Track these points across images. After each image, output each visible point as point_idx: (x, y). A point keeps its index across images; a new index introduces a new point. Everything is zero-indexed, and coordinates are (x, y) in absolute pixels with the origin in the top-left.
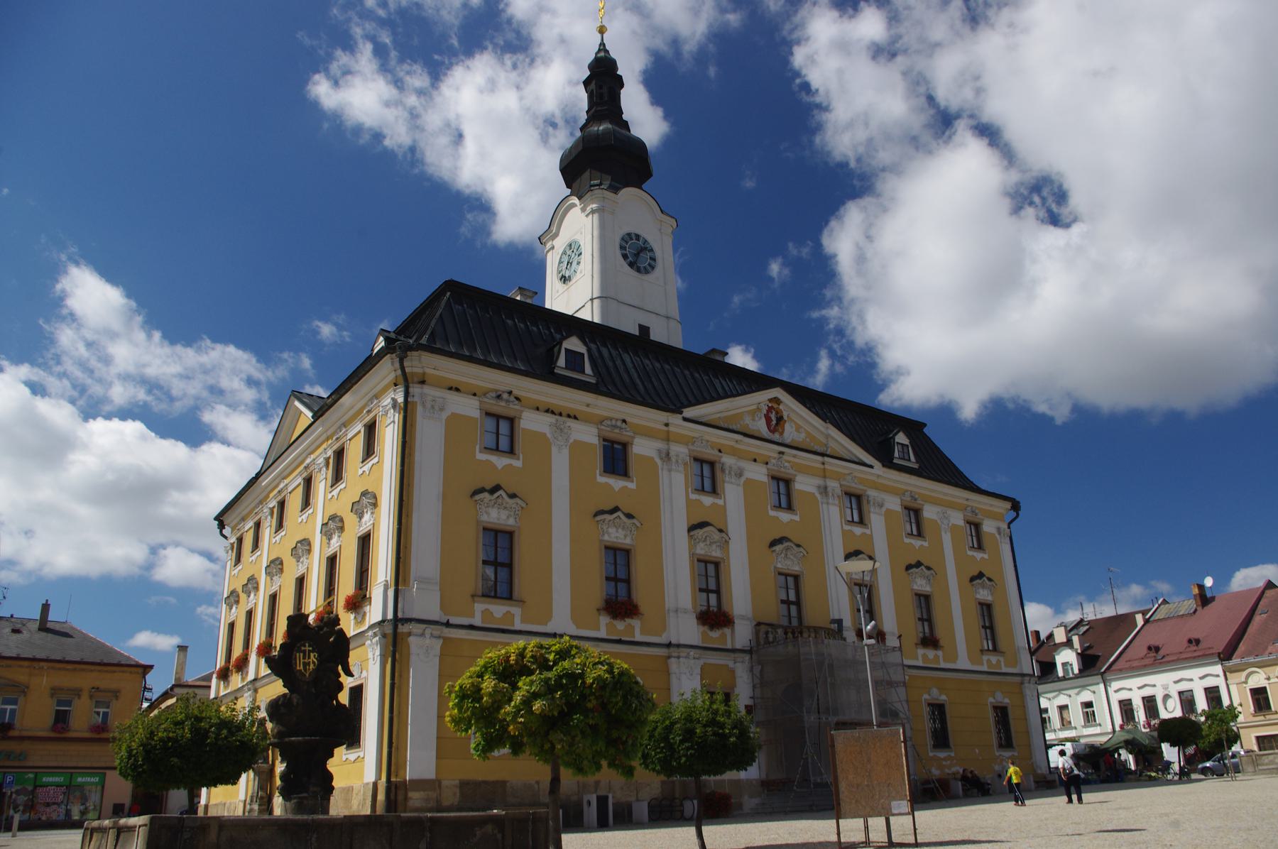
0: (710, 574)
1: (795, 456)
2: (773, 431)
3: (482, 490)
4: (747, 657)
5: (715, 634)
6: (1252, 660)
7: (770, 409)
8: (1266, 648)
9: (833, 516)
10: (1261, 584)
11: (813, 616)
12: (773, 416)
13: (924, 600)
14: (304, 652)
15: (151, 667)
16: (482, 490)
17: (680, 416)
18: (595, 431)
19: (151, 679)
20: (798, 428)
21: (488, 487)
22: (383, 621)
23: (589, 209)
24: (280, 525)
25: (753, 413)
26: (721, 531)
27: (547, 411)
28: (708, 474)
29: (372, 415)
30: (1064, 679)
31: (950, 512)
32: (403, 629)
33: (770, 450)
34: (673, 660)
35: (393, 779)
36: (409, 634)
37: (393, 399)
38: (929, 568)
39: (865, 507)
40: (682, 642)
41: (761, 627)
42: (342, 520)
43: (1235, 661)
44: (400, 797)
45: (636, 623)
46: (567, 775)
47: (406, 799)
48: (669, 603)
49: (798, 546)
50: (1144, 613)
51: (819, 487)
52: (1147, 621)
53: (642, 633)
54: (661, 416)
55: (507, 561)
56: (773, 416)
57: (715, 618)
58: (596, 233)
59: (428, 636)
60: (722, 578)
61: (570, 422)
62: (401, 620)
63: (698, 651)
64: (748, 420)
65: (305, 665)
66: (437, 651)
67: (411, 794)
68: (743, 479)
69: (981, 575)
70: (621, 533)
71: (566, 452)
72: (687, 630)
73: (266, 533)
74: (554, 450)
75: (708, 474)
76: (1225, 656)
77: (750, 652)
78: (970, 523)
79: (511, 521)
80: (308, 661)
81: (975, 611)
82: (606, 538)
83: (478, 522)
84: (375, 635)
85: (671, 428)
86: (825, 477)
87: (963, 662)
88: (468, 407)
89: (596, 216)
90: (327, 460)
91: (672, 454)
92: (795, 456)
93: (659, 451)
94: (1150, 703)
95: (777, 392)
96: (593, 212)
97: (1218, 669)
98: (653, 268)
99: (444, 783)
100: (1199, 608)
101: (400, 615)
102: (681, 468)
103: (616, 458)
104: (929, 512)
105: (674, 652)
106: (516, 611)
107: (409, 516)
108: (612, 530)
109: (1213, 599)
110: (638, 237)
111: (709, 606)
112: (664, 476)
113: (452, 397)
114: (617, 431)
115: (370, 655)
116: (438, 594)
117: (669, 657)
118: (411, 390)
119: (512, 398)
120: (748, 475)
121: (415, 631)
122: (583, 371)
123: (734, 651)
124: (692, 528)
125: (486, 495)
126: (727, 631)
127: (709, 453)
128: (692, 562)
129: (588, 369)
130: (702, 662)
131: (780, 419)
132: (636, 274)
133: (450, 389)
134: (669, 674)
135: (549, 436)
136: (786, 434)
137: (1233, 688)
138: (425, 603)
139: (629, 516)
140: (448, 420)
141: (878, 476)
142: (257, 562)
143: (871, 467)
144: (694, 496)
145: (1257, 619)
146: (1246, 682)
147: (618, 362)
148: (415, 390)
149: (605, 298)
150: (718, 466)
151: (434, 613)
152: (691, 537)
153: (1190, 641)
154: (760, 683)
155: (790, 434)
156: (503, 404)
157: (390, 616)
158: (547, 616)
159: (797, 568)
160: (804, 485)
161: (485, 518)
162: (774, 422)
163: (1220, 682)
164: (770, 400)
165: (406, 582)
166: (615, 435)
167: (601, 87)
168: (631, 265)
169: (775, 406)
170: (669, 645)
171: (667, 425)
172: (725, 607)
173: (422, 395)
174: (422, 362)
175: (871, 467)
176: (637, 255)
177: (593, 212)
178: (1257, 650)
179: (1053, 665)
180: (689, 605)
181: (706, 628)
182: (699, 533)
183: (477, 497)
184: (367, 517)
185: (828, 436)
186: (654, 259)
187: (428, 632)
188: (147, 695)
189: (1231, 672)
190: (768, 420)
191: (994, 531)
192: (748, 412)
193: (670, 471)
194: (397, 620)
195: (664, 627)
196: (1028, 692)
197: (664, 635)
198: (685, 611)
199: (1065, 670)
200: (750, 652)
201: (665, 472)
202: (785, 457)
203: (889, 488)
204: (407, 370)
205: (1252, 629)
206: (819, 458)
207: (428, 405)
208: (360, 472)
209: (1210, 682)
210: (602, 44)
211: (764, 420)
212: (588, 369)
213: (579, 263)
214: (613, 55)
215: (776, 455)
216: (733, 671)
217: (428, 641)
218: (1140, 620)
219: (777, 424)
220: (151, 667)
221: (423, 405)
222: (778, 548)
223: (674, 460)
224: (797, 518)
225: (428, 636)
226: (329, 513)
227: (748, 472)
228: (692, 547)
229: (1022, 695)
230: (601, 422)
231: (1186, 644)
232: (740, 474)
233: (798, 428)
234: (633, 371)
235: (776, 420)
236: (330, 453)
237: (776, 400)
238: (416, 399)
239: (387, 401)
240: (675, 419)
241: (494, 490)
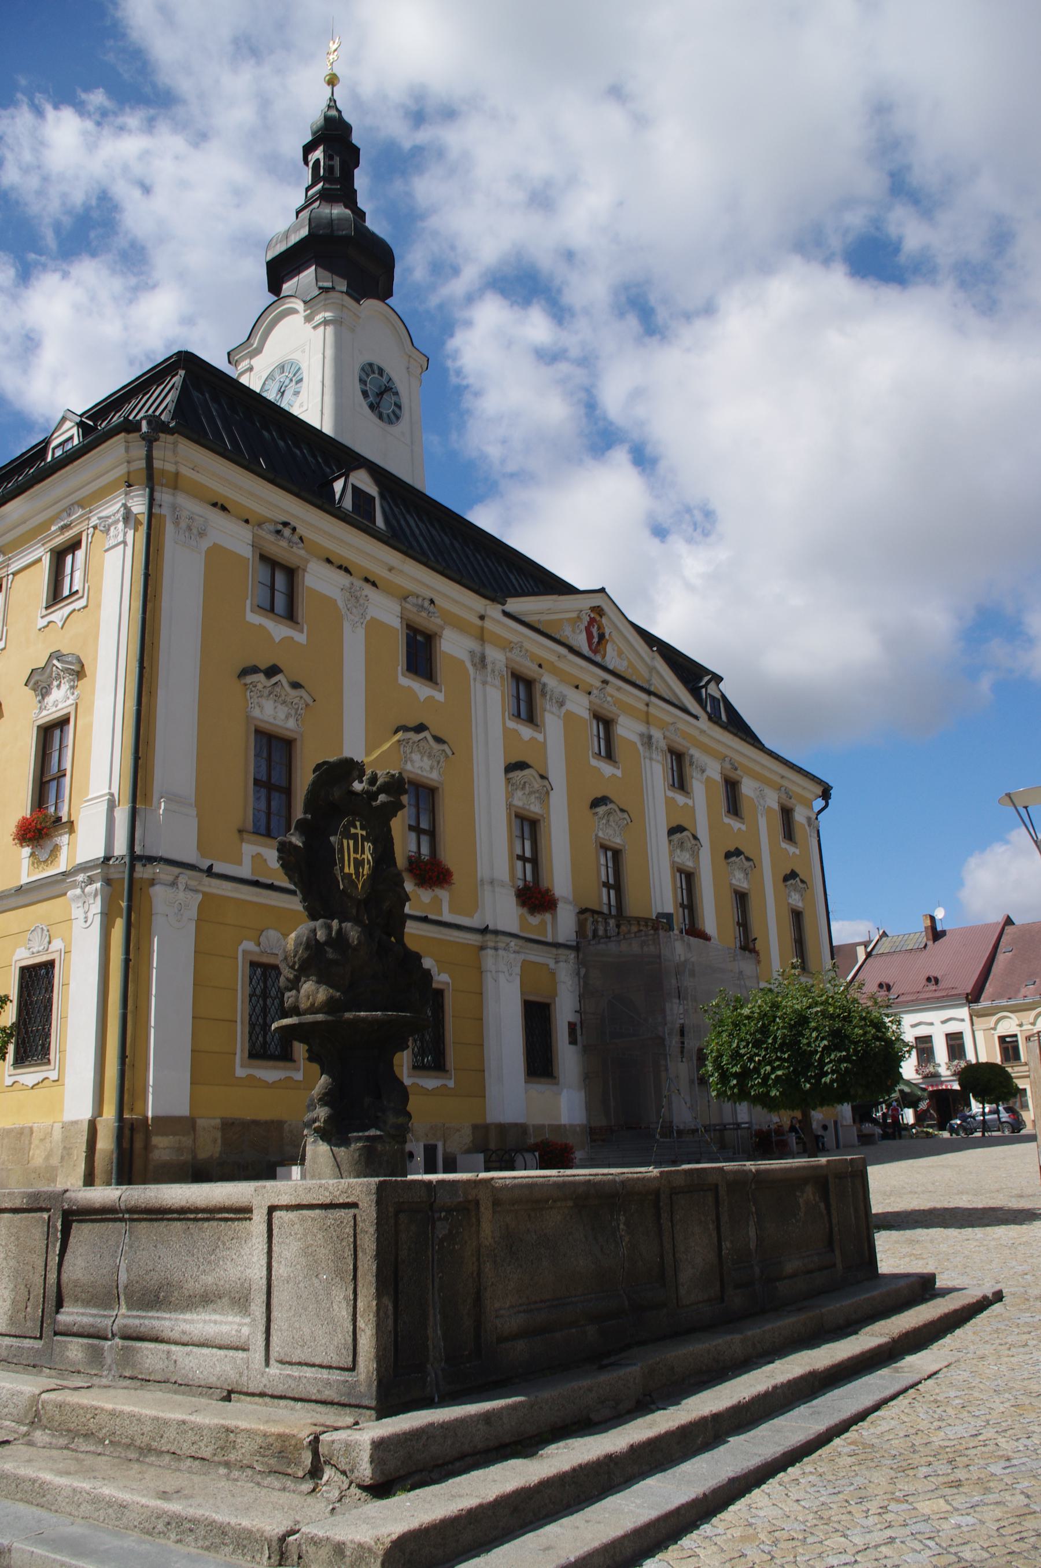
1: (619, 689)
2: (595, 652)
3: (254, 670)
4: (572, 955)
5: (534, 920)
6: (1004, 1002)
7: (592, 621)
8: (1018, 991)
10: (1000, 919)
11: (634, 908)
12: (595, 631)
13: (742, 898)
14: (355, 837)
16: (254, 670)
17: (500, 607)
18: (398, 609)
20: (620, 653)
22: (107, 859)
23: (319, 318)
26: (543, 777)
27: (340, 567)
29: (69, 534)
32: (142, 872)
33: (592, 676)
34: (490, 952)
35: (126, 1116)
36: (152, 882)
37: (125, 505)
38: (748, 859)
39: (687, 769)
40: (500, 928)
43: (984, 1004)
44: (138, 1145)
45: (443, 894)
47: (147, 1147)
48: (483, 871)
49: (622, 810)
51: (642, 735)
52: (869, 955)
53: (452, 910)
55: (284, 784)
57: (535, 898)
58: (330, 352)
59: (181, 887)
60: (542, 842)
61: (368, 590)
62: (140, 858)
63: (520, 942)
65: (359, 864)
66: (193, 913)
67: (156, 1140)
71: (361, 632)
72: (503, 911)
74: (347, 626)
75: (526, 697)
76: (973, 997)
77: (576, 948)
79: (291, 724)
83: (249, 718)
84: (91, 881)
85: (488, 624)
86: (648, 723)
88: (236, 539)
89: (330, 329)
91: (489, 660)
92: (619, 689)
93: (472, 653)
94: (955, 1044)
96: (326, 322)
97: (964, 1012)
98: (398, 418)
99: (201, 1122)
100: (930, 943)
101: (138, 850)
102: (497, 682)
107: (153, 694)
108: (416, 757)
109: (943, 933)
110: (381, 371)
111: (525, 880)
112: (476, 688)
113: (216, 517)
114: (424, 614)
115: (77, 912)
116: (195, 823)
117: (482, 948)
118: (157, 495)
119: (296, 539)
120: (569, 706)
121: (163, 876)
123: (557, 945)
124: (510, 768)
126: (548, 916)
127: (529, 668)
128: (509, 815)
130: (522, 957)
131: (602, 636)
132: (378, 421)
133: (215, 505)
135: (341, 604)
136: (608, 658)
137: (979, 1035)
138: (175, 834)
139: (438, 740)
141: (703, 732)
143: (696, 717)
145: (1001, 958)
146: (994, 1029)
147: (403, 522)
148: (164, 496)
150: (538, 688)
151: (190, 856)
152: (508, 780)
153: (929, 979)
154: (585, 993)
156: (284, 544)
157: (120, 848)
159: (618, 840)
161: (256, 713)
162: (596, 640)
163: (965, 1028)
164: (593, 609)
165: (147, 798)
166: (422, 620)
168: (372, 407)
169: (598, 618)
170: (485, 931)
171: (482, 618)
172: (545, 884)
173: (174, 507)
175: (696, 717)
176: (380, 395)
177: (326, 322)
178: (1008, 991)
181: (525, 911)
182: (517, 775)
183: (249, 679)
185: (652, 669)
187: (182, 880)
189: (979, 1016)
190: (590, 637)
192: (569, 620)
193: (484, 683)
194: (134, 858)
197: (476, 916)
200: (576, 948)
201: (479, 686)
202: (609, 689)
204: (157, 464)
205: (996, 969)
206: (644, 696)
207: (183, 525)
208: (43, 622)
209: (953, 1027)
210: (332, 100)
211: (584, 635)
213: (297, 393)
214: (346, 117)
215: (598, 684)
216: (553, 974)
219: (599, 643)
221: (176, 522)
222: (601, 810)
223: (489, 668)
224: (619, 773)
225: (181, 887)
228: (510, 795)
230: (405, 598)
231: (924, 982)
232: (561, 704)
233: (620, 653)
234: (421, 539)
238: (165, 511)
239: (113, 508)
240: (494, 611)
241: (272, 671)
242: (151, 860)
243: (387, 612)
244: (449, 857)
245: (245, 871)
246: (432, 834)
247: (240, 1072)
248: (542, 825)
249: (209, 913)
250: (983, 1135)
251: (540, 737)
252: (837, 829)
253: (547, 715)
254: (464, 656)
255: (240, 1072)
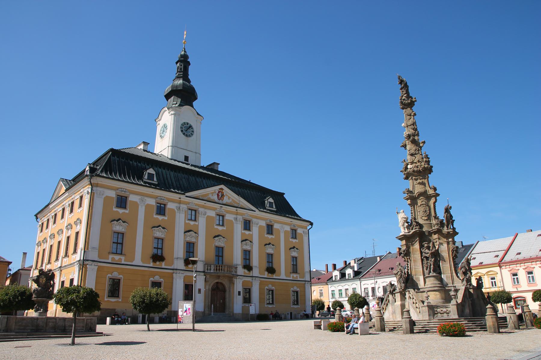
0: (190, 248)
2: (219, 200)
7: (219, 192)
9: (238, 228)
12: (220, 194)
15: (11, 262)
19: (10, 266)
20: (229, 198)
21: (116, 219)
24: (55, 222)
25: (212, 193)
28: (194, 214)
30: (335, 281)
31: (284, 226)
32: (86, 263)
41: (207, 264)
42: (72, 226)
45: (163, 263)
46: (396, 291)
48: (175, 256)
50: (380, 257)
52: (381, 260)
54: (178, 196)
56: (220, 194)
60: (195, 248)
64: (210, 196)
68: (206, 216)
69: (294, 247)
70: (161, 234)
71: (144, 207)
72: (180, 265)
73: (51, 223)
77: (204, 272)
78: (292, 230)
79: (123, 230)
80: (43, 280)
81: (290, 259)
82: (155, 235)
87: (283, 276)
90: (69, 204)
93: (177, 207)
95: (222, 186)
98: (192, 135)
103: (161, 210)
104: (276, 226)
105: (175, 271)
106: (123, 258)
110: (188, 124)
112: (177, 215)
122: (153, 180)
125: (115, 222)
129: (155, 179)
130: (183, 275)
134: (173, 278)
138: (93, 255)
140: (105, 198)
142: (47, 233)
144: (243, 232)
148: (94, 188)
149: (175, 146)
151: (96, 259)
152: (185, 235)
155: (226, 200)
157: (82, 259)
158: (133, 260)
160: (229, 217)
161: (114, 229)
167: (181, 66)
174: (96, 180)
179: (345, 274)
180: (182, 256)
182: (188, 234)
184: (78, 226)
185: (240, 201)
186: (193, 132)
188: (9, 272)
190: (218, 195)
191: (302, 232)
195: (173, 263)
196: (307, 287)
198: (180, 258)
199: (335, 279)
203: (260, 218)
206: (236, 209)
207: (98, 193)
212: (155, 179)
217: (93, 267)
218: (378, 259)
220: (11, 262)
222: (216, 238)
224: (225, 228)
226: (69, 223)
227: (209, 212)
229: (304, 287)
233: (229, 198)
235: (221, 195)
236: (70, 202)
237: (222, 189)
240: (183, 197)
242: (88, 260)
243: (288, 228)
244: (165, 255)
245: (110, 261)
246: (272, 262)
247: (106, 299)
248: (195, 245)
249: (99, 269)
250: (73, 341)
251: (251, 233)
252: (314, 235)
253: (254, 228)
254: (302, 232)
255: (106, 299)
